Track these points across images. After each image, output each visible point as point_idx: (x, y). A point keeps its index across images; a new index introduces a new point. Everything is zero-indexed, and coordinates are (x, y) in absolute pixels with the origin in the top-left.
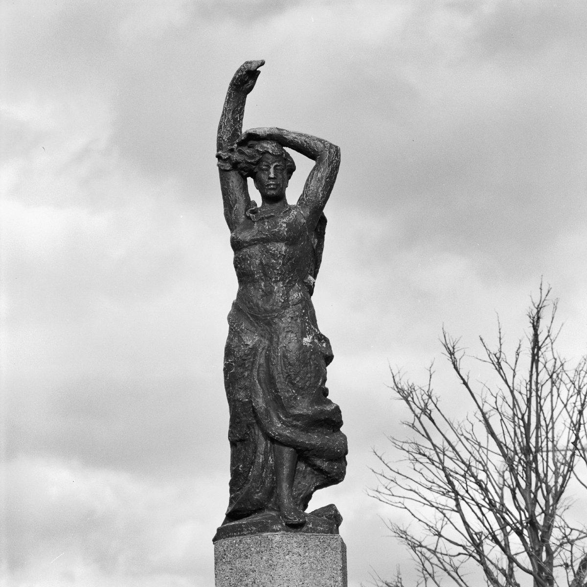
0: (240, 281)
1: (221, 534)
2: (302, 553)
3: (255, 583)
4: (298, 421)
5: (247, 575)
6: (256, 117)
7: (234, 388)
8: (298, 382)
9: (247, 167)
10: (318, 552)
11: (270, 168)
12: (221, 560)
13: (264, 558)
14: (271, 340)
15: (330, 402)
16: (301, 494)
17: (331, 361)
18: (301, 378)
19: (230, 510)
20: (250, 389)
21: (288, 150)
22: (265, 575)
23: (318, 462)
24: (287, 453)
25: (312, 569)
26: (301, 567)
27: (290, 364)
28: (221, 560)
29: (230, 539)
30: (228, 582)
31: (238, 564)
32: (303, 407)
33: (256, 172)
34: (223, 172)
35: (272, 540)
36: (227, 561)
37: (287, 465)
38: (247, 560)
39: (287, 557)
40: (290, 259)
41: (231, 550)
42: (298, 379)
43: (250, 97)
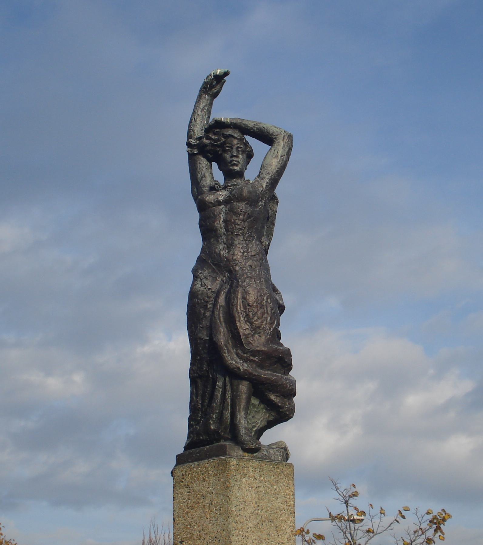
0: (204, 239)
1: (181, 460)
2: (257, 477)
3: (212, 504)
4: (255, 357)
5: (204, 497)
6: (223, 110)
7: (196, 327)
8: (255, 321)
9: (211, 149)
10: (272, 478)
11: (232, 148)
12: (179, 484)
13: (222, 480)
14: (230, 272)
15: (281, 345)
16: (255, 426)
17: (286, 420)
18: (258, 318)
19: (188, 442)
20: (212, 329)
21: (248, 138)
22: (221, 497)
23: (273, 397)
24: (244, 387)
25: (266, 492)
26: (256, 490)
27: (249, 304)
28: (179, 484)
29: (188, 464)
30: (186, 504)
31: (196, 487)
32: (259, 342)
33: (221, 154)
34: (192, 157)
35: (229, 462)
36: (185, 485)
37: (244, 396)
38: (204, 483)
39: (244, 480)
40: (249, 217)
41: (189, 474)
42: (256, 318)
43: (215, 100)
